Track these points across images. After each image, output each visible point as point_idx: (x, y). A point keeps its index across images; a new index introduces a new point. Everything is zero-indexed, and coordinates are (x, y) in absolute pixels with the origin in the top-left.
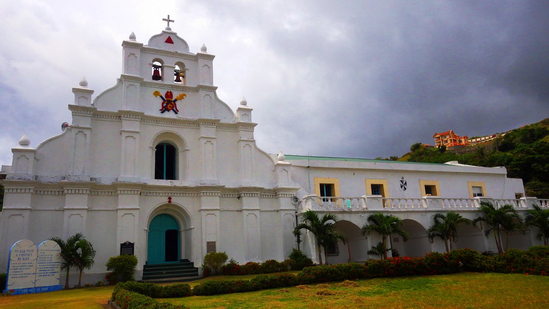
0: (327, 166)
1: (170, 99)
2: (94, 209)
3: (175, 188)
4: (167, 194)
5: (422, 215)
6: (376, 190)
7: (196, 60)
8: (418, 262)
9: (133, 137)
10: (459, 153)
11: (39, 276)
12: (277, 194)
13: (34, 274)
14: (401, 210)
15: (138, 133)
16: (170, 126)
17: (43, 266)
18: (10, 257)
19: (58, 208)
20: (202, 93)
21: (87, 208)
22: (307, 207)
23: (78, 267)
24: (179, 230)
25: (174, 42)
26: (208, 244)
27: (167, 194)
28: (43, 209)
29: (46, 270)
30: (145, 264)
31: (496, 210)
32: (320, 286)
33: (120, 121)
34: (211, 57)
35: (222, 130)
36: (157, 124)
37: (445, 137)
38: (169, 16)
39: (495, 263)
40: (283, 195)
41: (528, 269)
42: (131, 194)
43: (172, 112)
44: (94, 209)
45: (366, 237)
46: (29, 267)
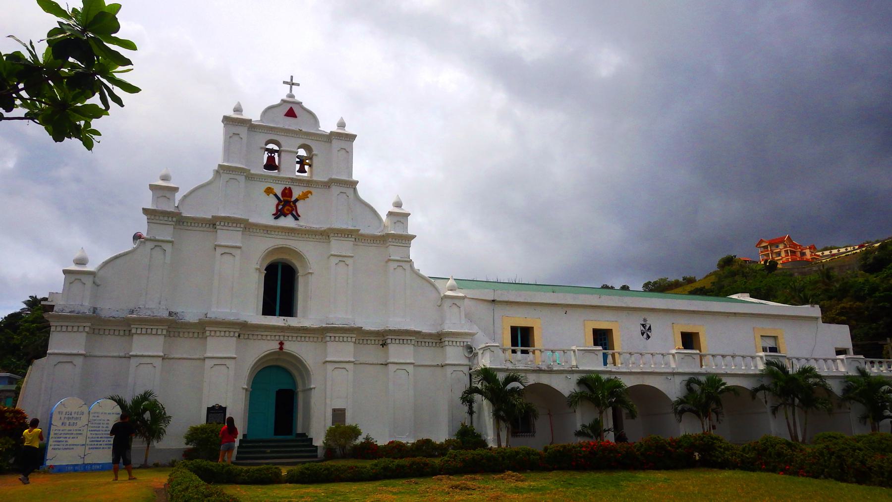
3: (290, 329)
4: (277, 337)
6: (603, 337)
8: (625, 449)
9: (231, 254)
11: (89, 448)
12: (442, 340)
13: (83, 445)
14: (633, 371)
15: (239, 248)
17: (96, 434)
19: (122, 354)
20: (335, 190)
22: (485, 361)
23: (145, 439)
24: (296, 390)
25: (297, 115)
26: (335, 411)
27: (277, 337)
28: (103, 354)
29: (100, 441)
31: (790, 375)
32: (466, 478)
33: (215, 230)
34: (352, 137)
37: (777, 247)
38: (292, 77)
39: (742, 455)
40: (450, 343)
41: (783, 466)
43: (290, 217)
45: (573, 410)
46: (75, 436)
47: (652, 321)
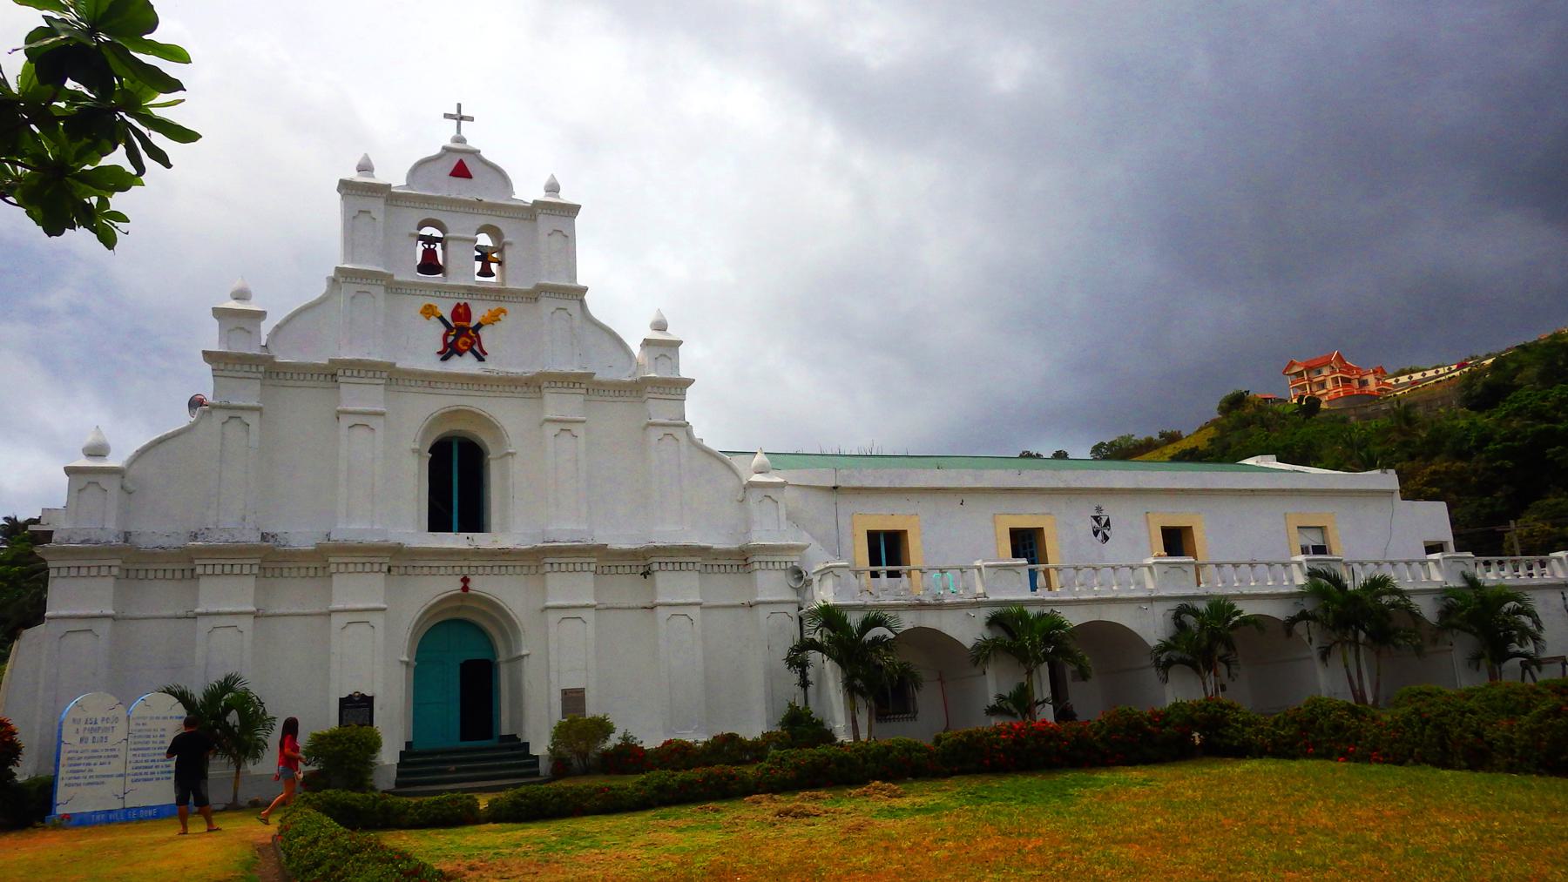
0: (885, 484)
1: (465, 324)
2: (273, 612)
3: (478, 553)
4: (457, 569)
5: (1140, 608)
7: (533, 217)
8: (1074, 733)
10: (1359, 417)
12: (749, 561)
13: (120, 775)
14: (1081, 597)
15: (382, 414)
16: (465, 393)
18: (60, 736)
19: (181, 612)
20: (547, 305)
21: (254, 609)
22: (825, 594)
23: (231, 759)
27: (457, 569)
29: (151, 767)
30: (404, 750)
32: (803, 797)
34: (572, 210)
35: (600, 399)
36: (431, 390)
38: (471, 119)
39: (1273, 733)
41: (1344, 747)
42: (363, 572)
43: (469, 357)
44: (271, 612)
46: (107, 760)
47: (1111, 510)
